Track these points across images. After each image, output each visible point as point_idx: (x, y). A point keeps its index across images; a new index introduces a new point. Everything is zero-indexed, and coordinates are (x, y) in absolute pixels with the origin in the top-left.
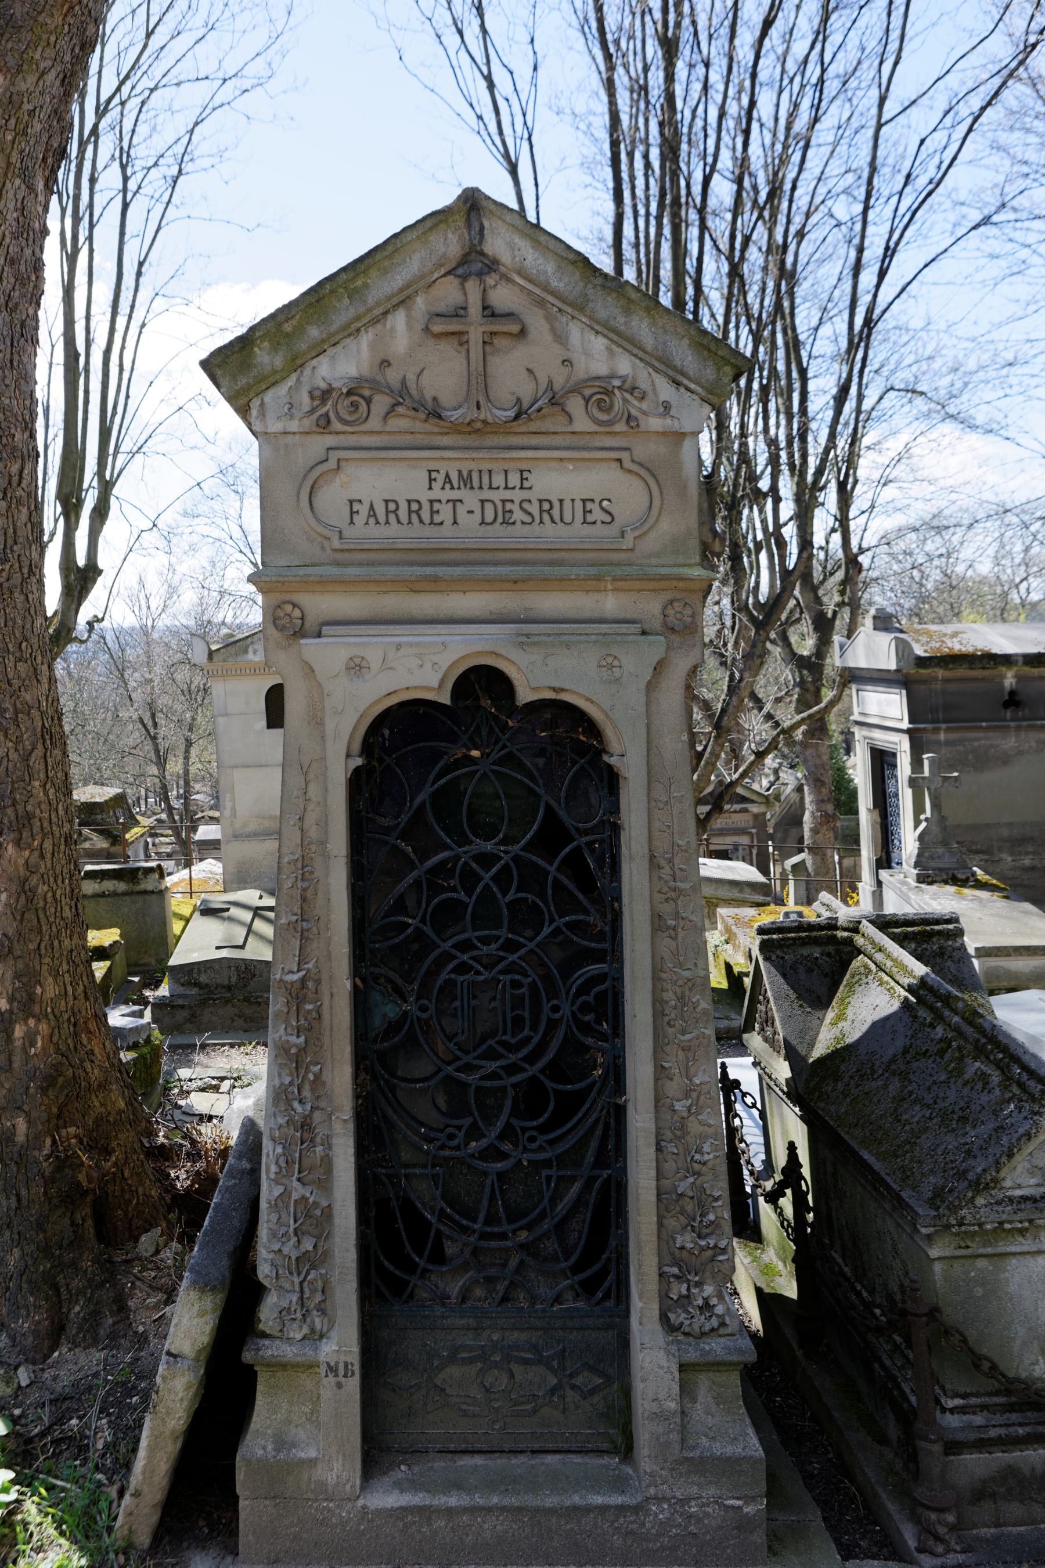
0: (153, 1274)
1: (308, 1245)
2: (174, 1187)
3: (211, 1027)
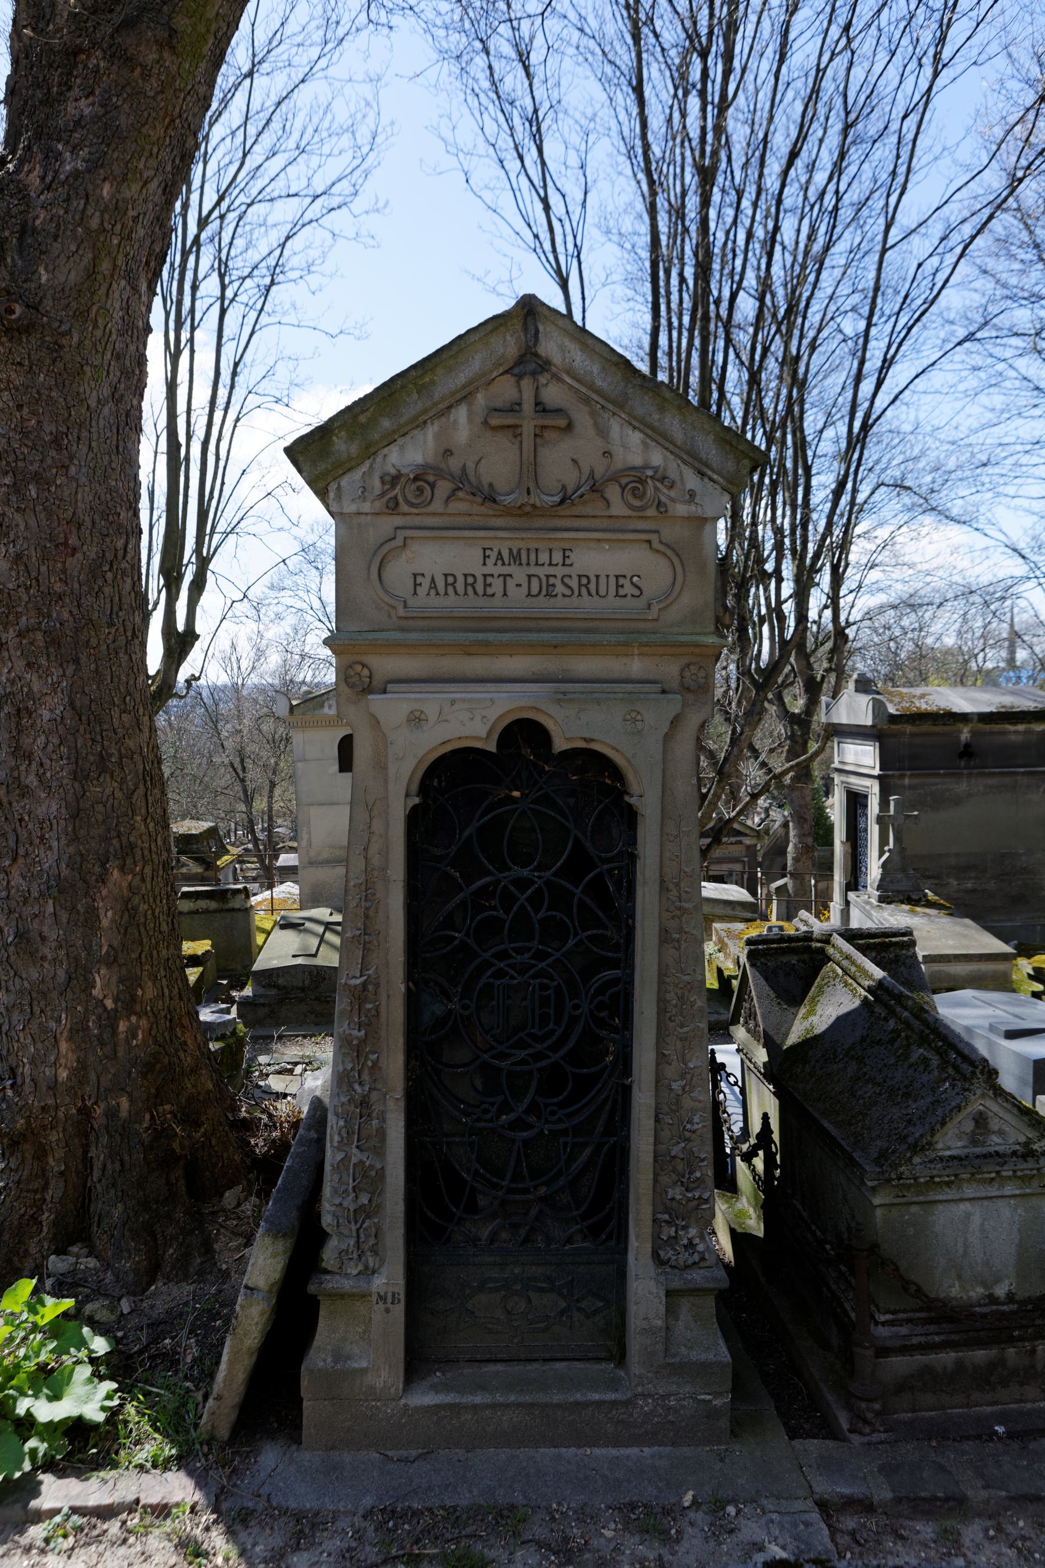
1: (364, 1199)
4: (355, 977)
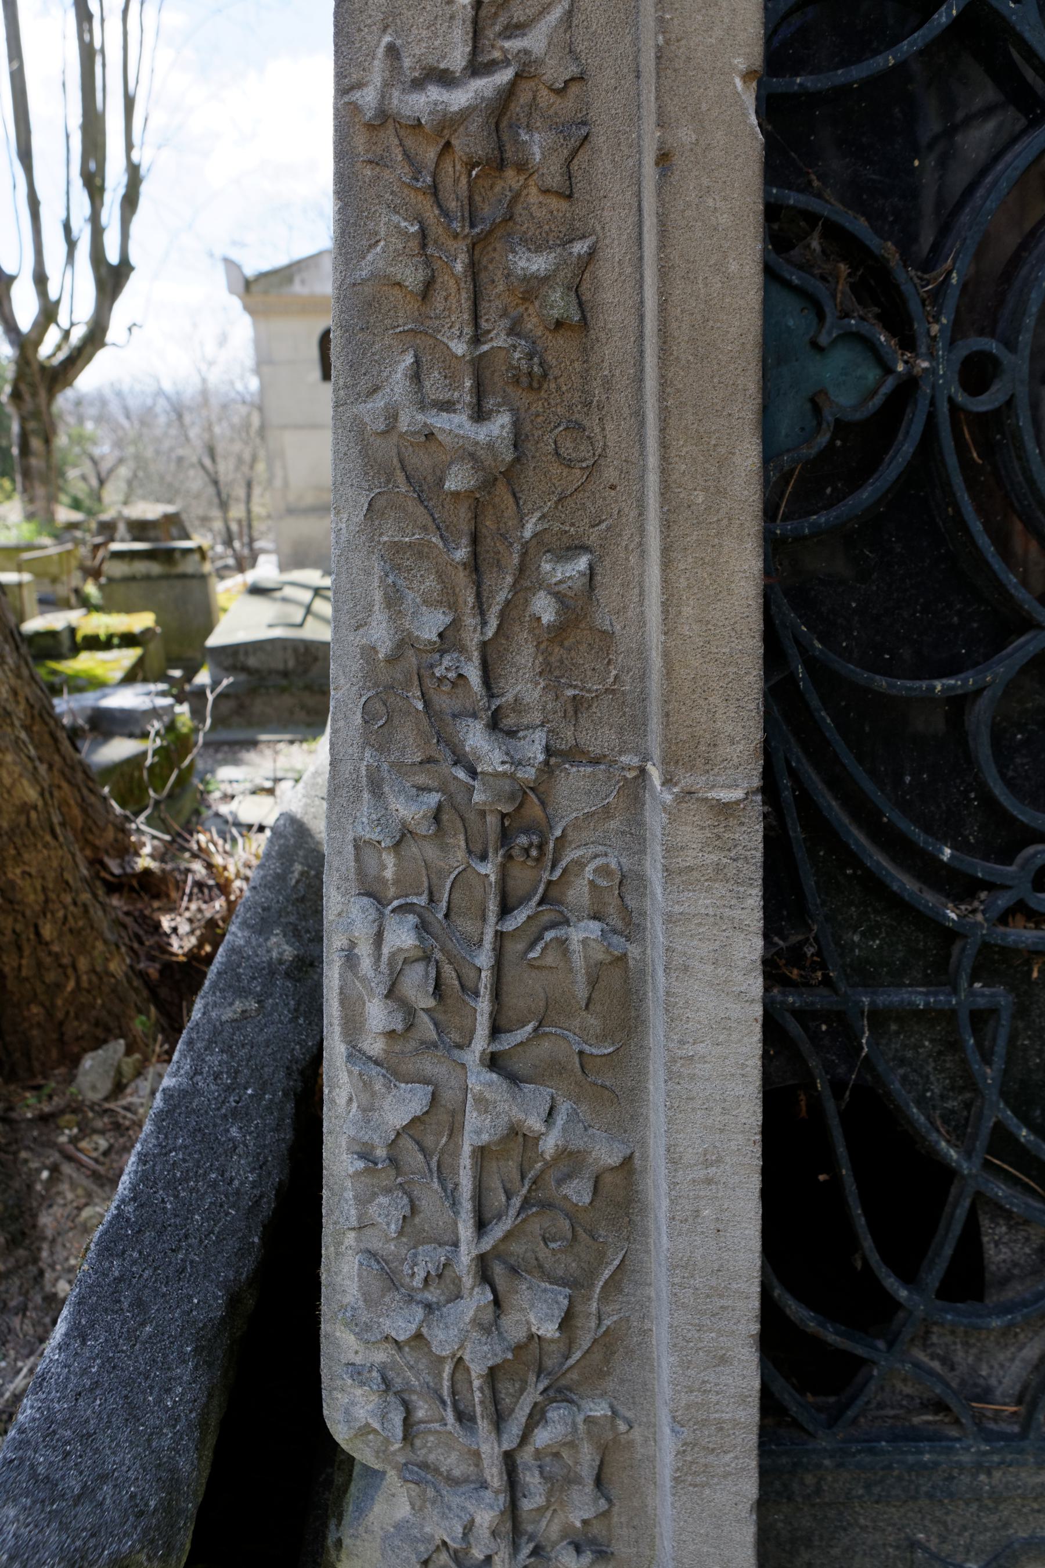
0: (103, 1143)
1: (537, 1315)
2: (164, 948)
3: (265, 725)
4: (445, 79)
